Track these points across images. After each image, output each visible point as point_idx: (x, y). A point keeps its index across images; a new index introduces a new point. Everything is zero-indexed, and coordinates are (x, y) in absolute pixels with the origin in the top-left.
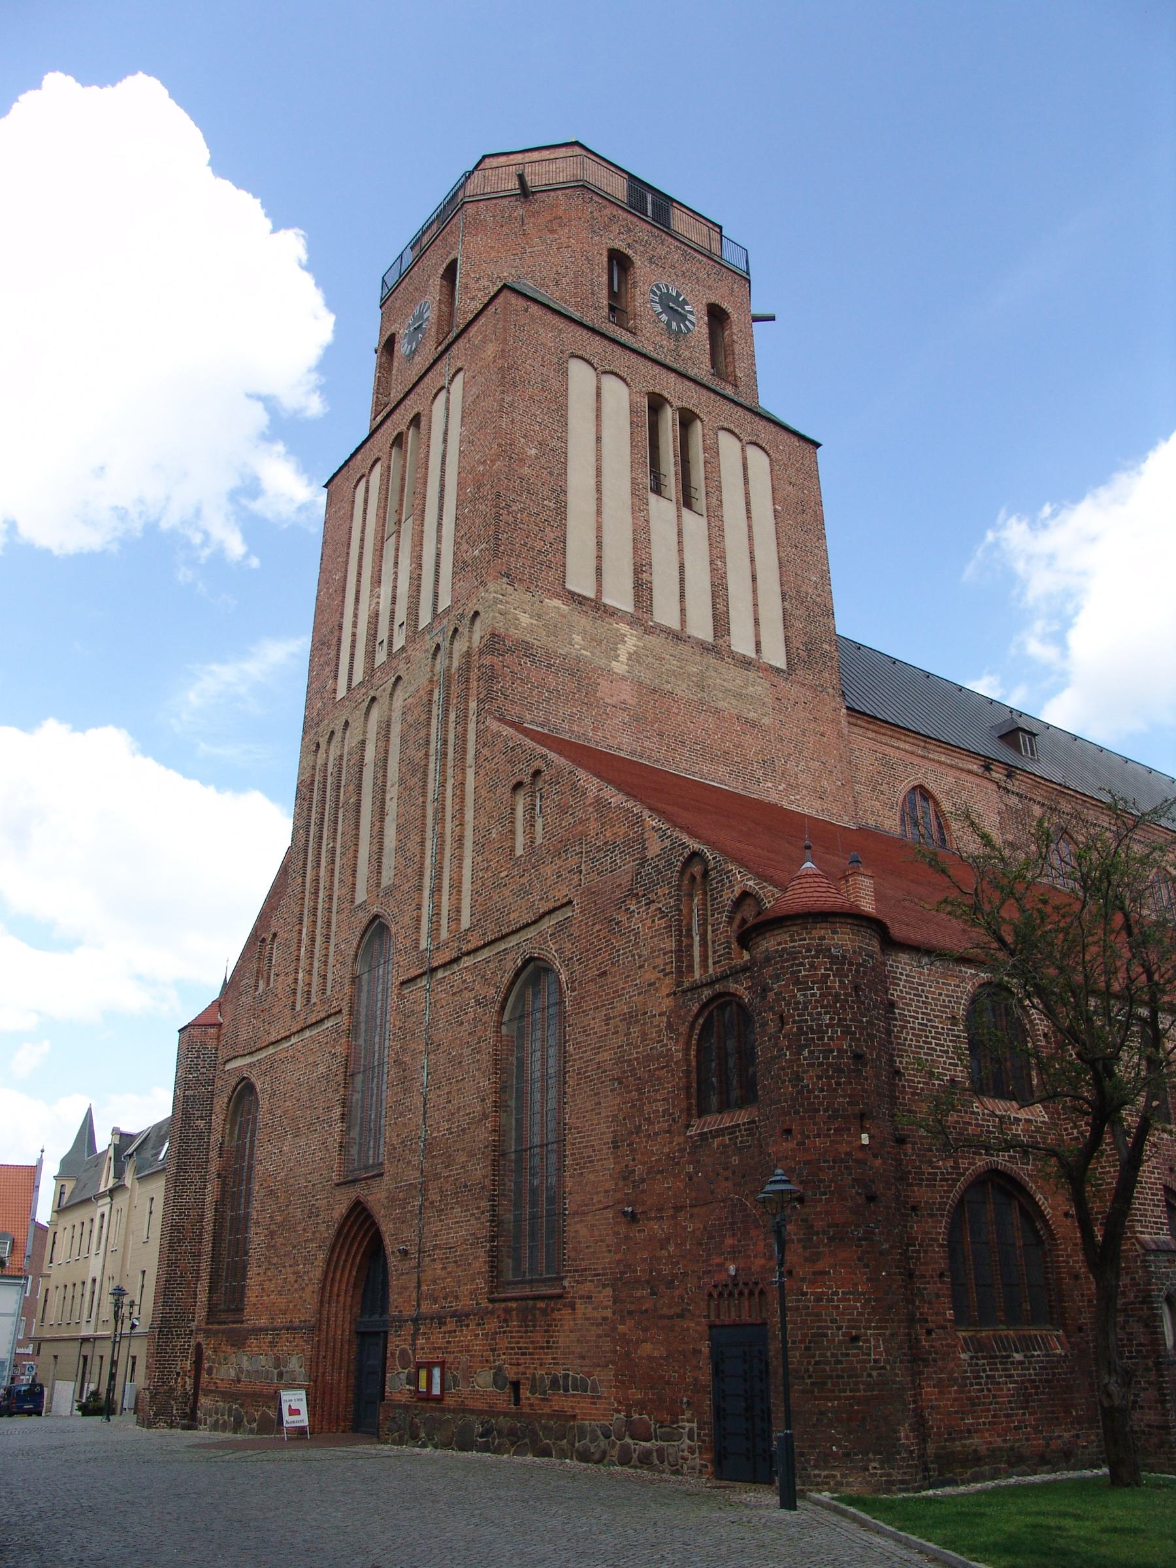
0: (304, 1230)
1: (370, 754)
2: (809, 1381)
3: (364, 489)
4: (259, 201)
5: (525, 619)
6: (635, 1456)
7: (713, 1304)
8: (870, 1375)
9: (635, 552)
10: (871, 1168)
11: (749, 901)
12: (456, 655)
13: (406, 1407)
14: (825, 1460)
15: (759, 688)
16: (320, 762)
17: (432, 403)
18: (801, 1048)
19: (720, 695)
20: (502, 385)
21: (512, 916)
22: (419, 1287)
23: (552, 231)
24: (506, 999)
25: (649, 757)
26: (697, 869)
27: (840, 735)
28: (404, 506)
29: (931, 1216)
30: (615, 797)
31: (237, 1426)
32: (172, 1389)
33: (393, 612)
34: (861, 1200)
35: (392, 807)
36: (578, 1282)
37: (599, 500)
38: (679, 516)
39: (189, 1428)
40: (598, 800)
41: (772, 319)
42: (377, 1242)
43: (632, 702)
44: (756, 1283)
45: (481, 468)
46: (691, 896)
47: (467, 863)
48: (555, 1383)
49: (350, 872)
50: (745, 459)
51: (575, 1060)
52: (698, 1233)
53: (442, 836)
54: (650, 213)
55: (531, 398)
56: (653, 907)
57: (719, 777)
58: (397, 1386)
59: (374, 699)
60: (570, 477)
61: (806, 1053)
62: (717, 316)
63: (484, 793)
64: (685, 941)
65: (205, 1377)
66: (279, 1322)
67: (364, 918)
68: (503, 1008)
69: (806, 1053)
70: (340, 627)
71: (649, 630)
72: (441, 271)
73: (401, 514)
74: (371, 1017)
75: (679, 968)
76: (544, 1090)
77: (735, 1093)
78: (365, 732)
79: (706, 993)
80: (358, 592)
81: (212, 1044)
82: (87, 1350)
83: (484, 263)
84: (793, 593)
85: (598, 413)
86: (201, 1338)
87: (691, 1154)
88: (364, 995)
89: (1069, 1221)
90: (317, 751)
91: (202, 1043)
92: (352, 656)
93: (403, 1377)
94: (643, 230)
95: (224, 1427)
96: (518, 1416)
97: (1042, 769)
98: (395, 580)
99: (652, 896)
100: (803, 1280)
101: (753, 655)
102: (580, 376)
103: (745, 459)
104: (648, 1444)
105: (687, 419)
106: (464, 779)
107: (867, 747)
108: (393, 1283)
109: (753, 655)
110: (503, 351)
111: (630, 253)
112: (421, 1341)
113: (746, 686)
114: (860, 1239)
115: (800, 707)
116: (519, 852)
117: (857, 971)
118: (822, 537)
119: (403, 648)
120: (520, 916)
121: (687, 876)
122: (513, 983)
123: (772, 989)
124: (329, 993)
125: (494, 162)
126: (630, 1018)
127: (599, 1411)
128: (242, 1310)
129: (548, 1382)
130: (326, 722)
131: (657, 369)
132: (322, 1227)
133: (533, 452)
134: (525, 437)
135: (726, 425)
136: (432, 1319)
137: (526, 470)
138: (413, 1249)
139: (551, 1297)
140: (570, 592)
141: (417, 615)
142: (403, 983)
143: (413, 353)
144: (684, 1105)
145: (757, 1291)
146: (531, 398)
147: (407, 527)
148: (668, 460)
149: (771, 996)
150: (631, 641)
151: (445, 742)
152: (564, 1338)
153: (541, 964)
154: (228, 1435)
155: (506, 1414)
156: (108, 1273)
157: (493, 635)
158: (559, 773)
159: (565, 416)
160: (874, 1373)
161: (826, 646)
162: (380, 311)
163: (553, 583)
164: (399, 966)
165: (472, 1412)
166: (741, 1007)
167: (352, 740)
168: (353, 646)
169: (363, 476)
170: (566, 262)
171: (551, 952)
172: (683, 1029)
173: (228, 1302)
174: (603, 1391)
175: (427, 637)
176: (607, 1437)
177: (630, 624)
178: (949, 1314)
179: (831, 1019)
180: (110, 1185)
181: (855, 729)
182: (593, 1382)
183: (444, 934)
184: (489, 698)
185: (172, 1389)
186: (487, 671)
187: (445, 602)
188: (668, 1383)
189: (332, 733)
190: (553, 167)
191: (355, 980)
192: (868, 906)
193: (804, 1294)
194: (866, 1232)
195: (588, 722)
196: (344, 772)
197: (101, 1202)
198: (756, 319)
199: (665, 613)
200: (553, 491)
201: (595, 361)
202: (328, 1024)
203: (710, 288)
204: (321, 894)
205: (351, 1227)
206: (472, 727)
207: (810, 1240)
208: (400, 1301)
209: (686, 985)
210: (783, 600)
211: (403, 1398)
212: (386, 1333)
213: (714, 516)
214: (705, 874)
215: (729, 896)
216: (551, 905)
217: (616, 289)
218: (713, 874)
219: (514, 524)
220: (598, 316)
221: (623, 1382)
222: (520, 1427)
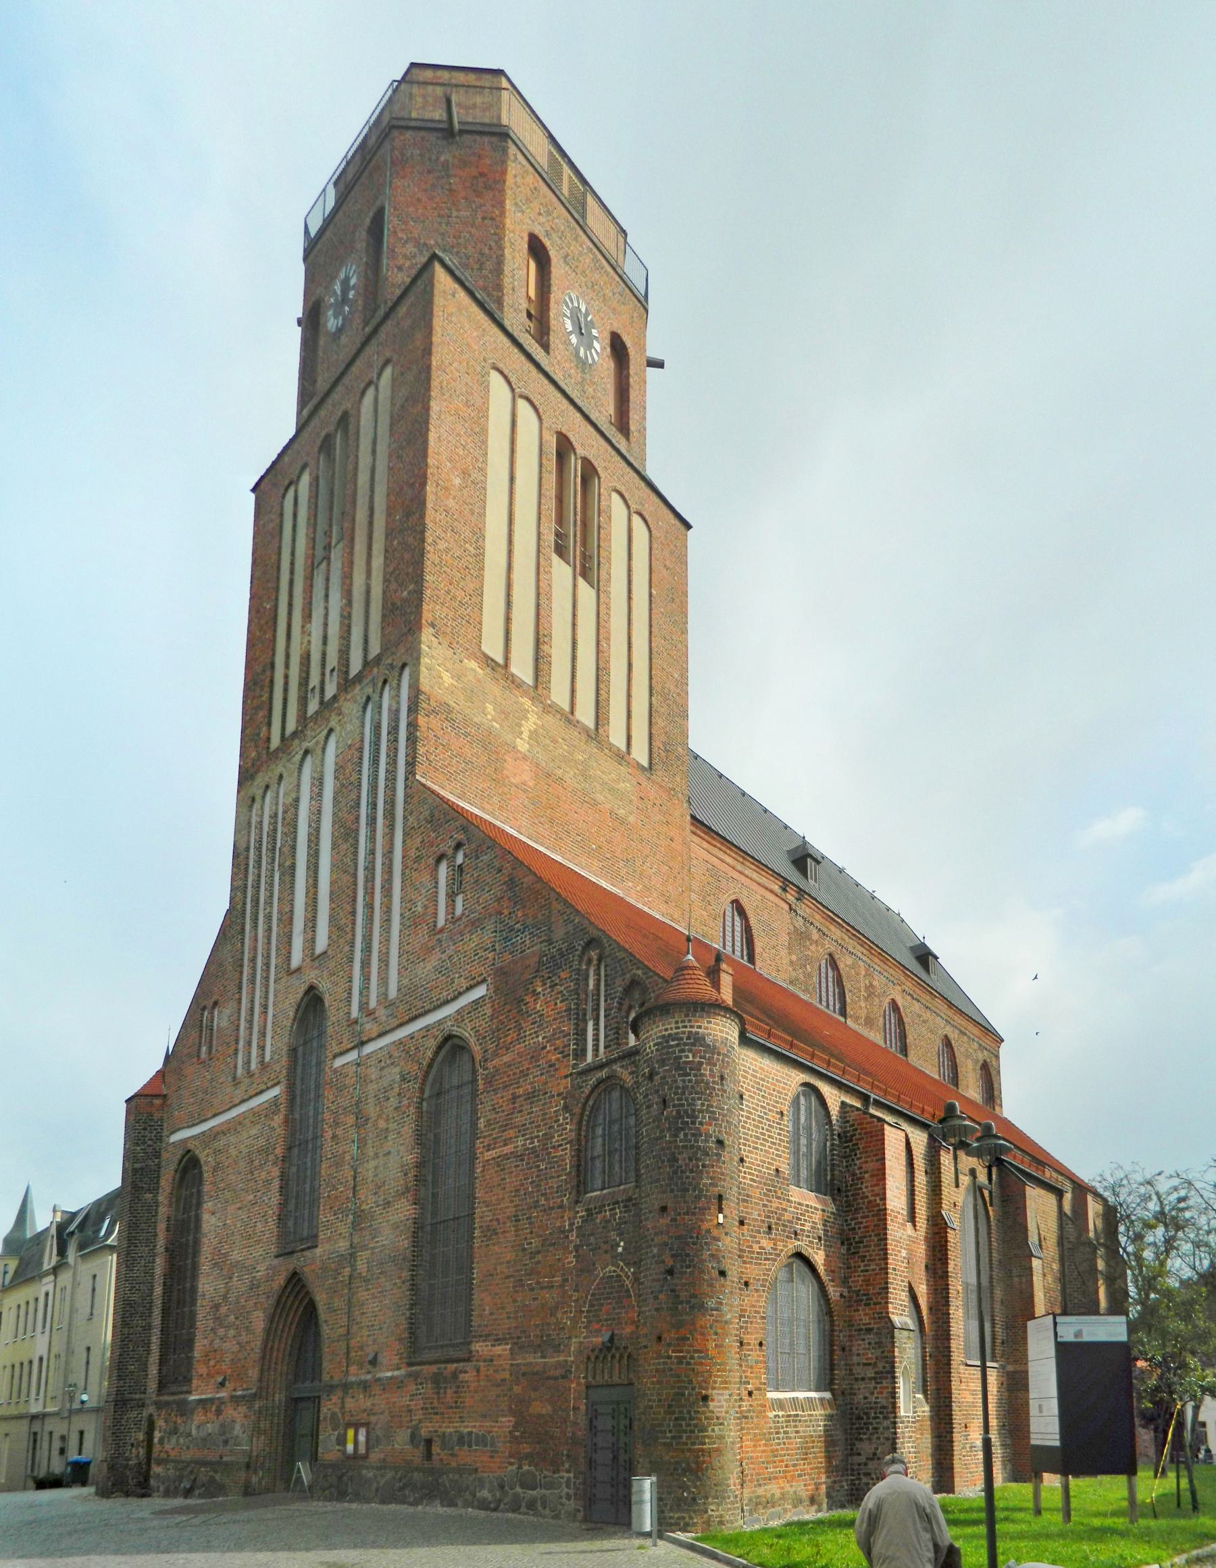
2: (669, 1435)
5: (447, 679)
7: (591, 1366)
29: (757, 1291)
33: (324, 654)
42: (311, 1311)
43: (531, 784)
51: (485, 1137)
70: (273, 666)
73: (331, 537)
82: (36, 1427)
86: (152, 1409)
90: (251, 807)
91: (147, 1113)
92: (285, 700)
93: (334, 1438)
100: (669, 1345)
104: (534, 1493)
115: (656, 809)
116: (441, 922)
118: (684, 632)
121: (585, 958)
123: (657, 1073)
129: (455, 1438)
132: (263, 1299)
133: (457, 481)
135: (618, 487)
141: (348, 660)
143: (340, 330)
144: (574, 1182)
147: (336, 555)
149: (657, 1078)
153: (456, 1041)
156: (54, 1351)
159: (485, 442)
163: (470, 641)
168: (286, 690)
172: (577, 1110)
180: (53, 1263)
181: (696, 839)
182: (492, 1437)
193: (669, 1357)
197: (45, 1280)
199: (559, 695)
208: (331, 1369)
212: (319, 1397)
221: (516, 1438)
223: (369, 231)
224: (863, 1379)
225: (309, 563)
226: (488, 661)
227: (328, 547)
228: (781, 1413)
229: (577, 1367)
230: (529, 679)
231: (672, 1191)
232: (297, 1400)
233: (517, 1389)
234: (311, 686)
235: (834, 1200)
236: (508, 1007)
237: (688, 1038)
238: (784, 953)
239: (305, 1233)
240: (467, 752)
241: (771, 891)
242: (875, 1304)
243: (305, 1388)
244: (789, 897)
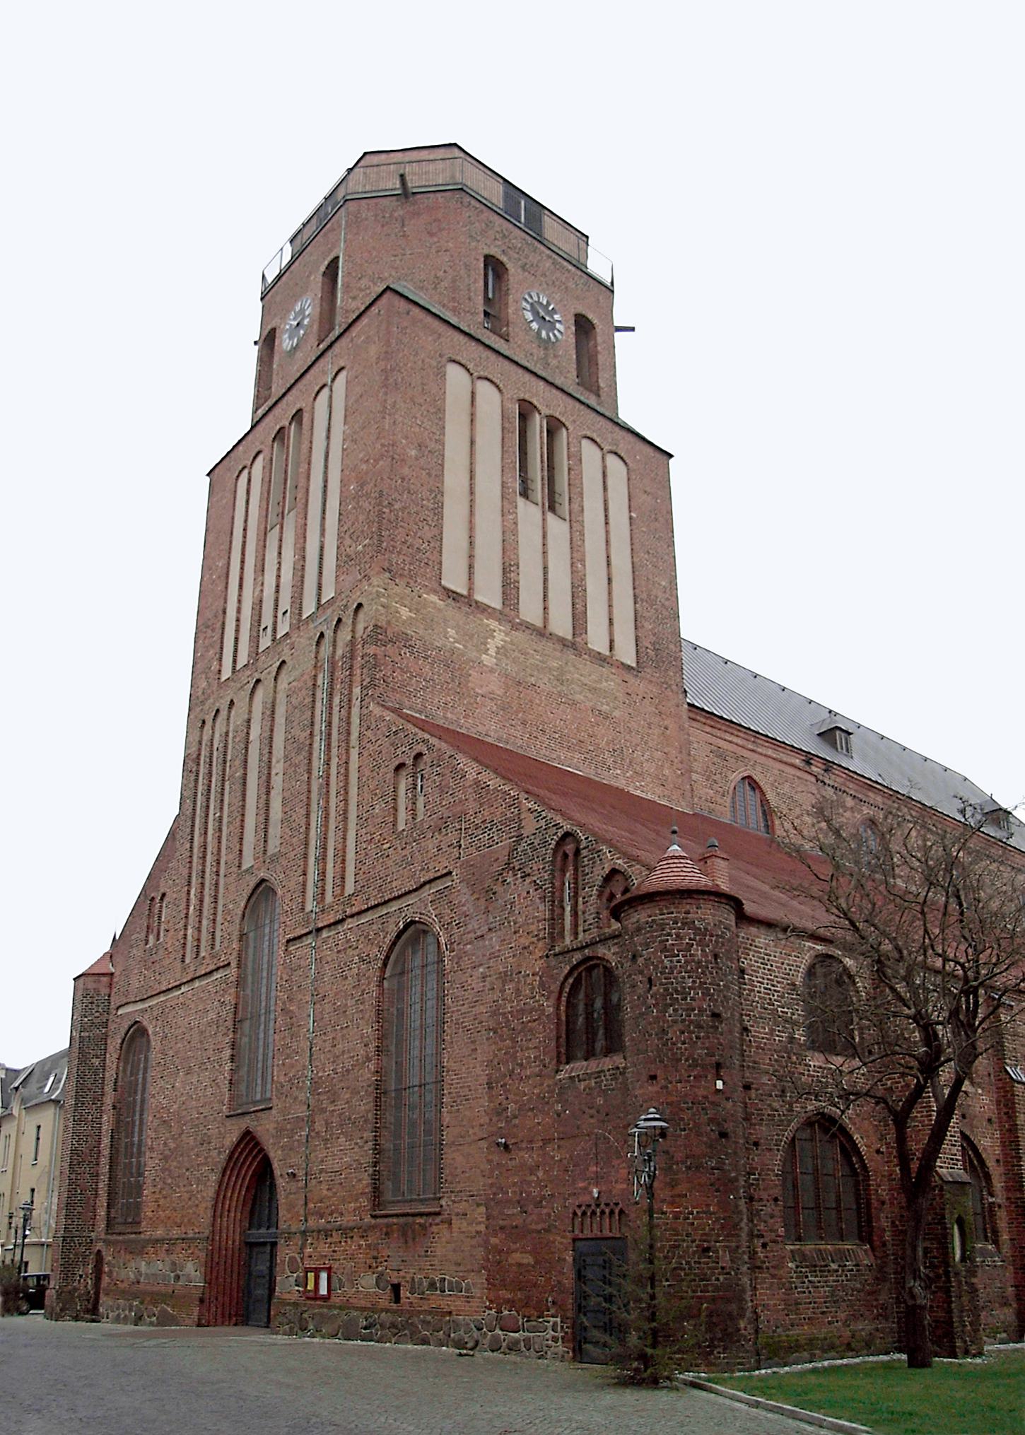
0: (197, 1155)
3: (246, 480)
5: (405, 613)
6: (504, 1344)
8: (718, 1279)
10: (724, 1109)
11: (618, 877)
12: (340, 644)
13: (295, 1305)
15: (611, 682)
16: (206, 738)
17: (315, 399)
19: (578, 689)
20: (386, 386)
21: (394, 884)
23: (431, 234)
24: (387, 957)
26: (569, 848)
27: (681, 728)
28: (286, 498)
30: (494, 782)
31: (138, 1320)
33: (277, 600)
34: (715, 1136)
35: (277, 782)
36: (454, 1202)
39: (93, 1321)
40: (477, 782)
41: (632, 329)
42: (266, 1165)
43: (500, 692)
44: (617, 1204)
45: (364, 467)
46: (563, 871)
48: (432, 1285)
49: (237, 839)
52: (565, 1162)
53: (326, 809)
54: (523, 219)
56: (528, 880)
57: (574, 763)
58: (287, 1286)
59: (258, 681)
62: (583, 326)
63: (367, 773)
64: (557, 911)
65: (105, 1280)
66: (175, 1233)
68: (385, 964)
71: (515, 627)
72: (323, 269)
73: (284, 507)
74: (257, 970)
75: (551, 934)
76: (423, 1038)
77: (600, 1043)
78: (250, 712)
79: (577, 957)
81: (104, 991)
83: (366, 264)
84: (644, 596)
85: (472, 418)
87: (559, 1094)
88: (251, 951)
89: (879, 1157)
91: (94, 992)
93: (292, 1280)
95: (126, 1320)
97: (855, 765)
99: (528, 870)
101: (608, 653)
105: (554, 426)
106: (348, 758)
109: (608, 653)
110: (386, 352)
111: (504, 259)
112: (308, 1250)
113: (600, 681)
114: (713, 1168)
115: (647, 701)
120: (399, 886)
122: (394, 944)
124: (217, 947)
125: (375, 159)
126: (505, 977)
127: (471, 1306)
128: (139, 1223)
130: (211, 700)
131: (527, 376)
132: (214, 1153)
133: (413, 453)
134: (407, 438)
135: (589, 434)
136: (319, 1231)
137: (406, 471)
138: (301, 1173)
140: (445, 588)
142: (288, 941)
143: (295, 349)
145: (617, 1211)
148: (536, 465)
149: (640, 961)
150: (500, 636)
151: (329, 724)
152: (440, 1250)
153: (421, 927)
154: (130, 1327)
155: (387, 1311)
157: (376, 626)
159: (442, 419)
161: (672, 646)
162: (260, 305)
164: (284, 923)
165: (357, 1309)
166: (608, 971)
167: (238, 716)
169: (244, 468)
170: (442, 266)
171: (431, 915)
172: (555, 987)
173: (125, 1215)
174: (476, 1292)
175: (312, 626)
176: (479, 1329)
177: (499, 620)
178: (781, 1231)
179: (694, 982)
181: (695, 724)
183: (329, 898)
184: (372, 685)
186: (363, 658)
187: (328, 594)
189: (218, 711)
190: (431, 167)
191: (242, 937)
192: (725, 887)
193: (664, 1213)
195: (460, 709)
196: (230, 747)
198: (619, 329)
199: (530, 610)
201: (470, 366)
202: (217, 975)
203: (577, 298)
204: (209, 857)
205: (241, 1153)
206: (355, 711)
207: (671, 1168)
208: (287, 1218)
209: (557, 949)
211: (294, 1298)
212: (274, 1244)
214: (577, 852)
215: (598, 874)
216: (431, 875)
217: (490, 296)
218: (584, 853)
219: (392, 523)
220: (474, 322)
222: (398, 1318)
225: (262, 527)
226: (451, 595)
227: (282, 515)
230: (496, 603)
232: (251, 1245)
233: (494, 1240)
234: (263, 626)
239: (258, 1097)
241: (792, 765)
243: (261, 1233)
244: (814, 768)
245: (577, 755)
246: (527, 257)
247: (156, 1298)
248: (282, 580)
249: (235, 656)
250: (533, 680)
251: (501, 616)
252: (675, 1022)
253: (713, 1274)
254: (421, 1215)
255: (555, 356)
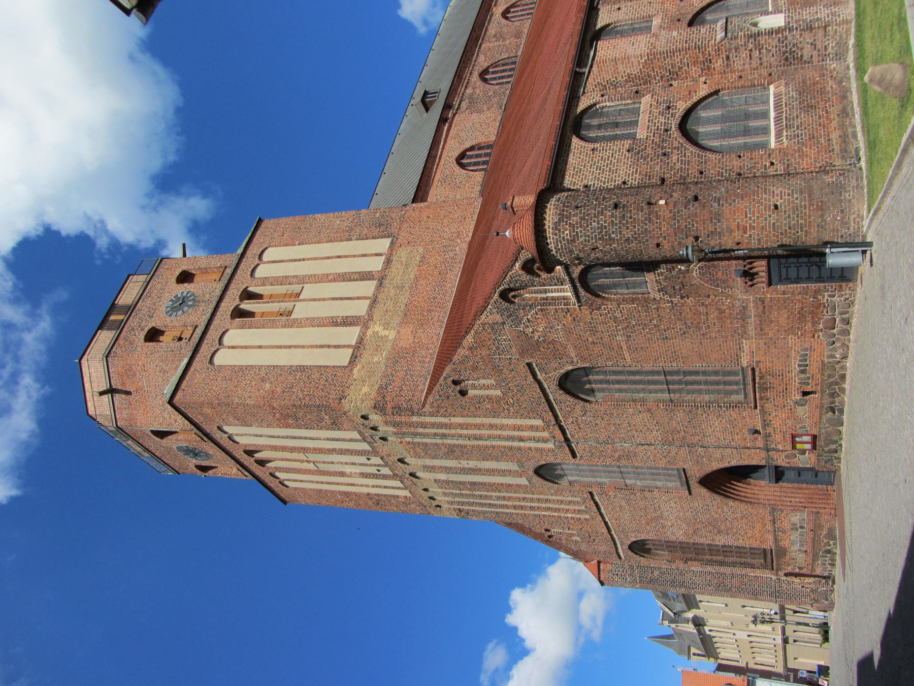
1: (443, 477)
4: (511, 620)
5: (365, 389)
6: (844, 327)
9: (326, 326)
14: (844, 223)
15: (402, 254)
18: (610, 239)
22: (748, 448)
23: (134, 375)
25: (444, 317)
29: (706, 163)
32: (812, 591)
34: (697, 204)
35: (472, 464)
37: (295, 347)
38: (304, 300)
45: (277, 415)
47: (505, 421)
50: (269, 262)
55: (235, 387)
58: (807, 460)
60: (282, 364)
61: (613, 236)
65: (804, 571)
66: (769, 527)
67: (536, 480)
69: (613, 236)
72: (158, 439)
80: (348, 484)
86: (781, 573)
92: (386, 487)
93: (801, 457)
94: (133, 322)
96: (823, 392)
98: (342, 463)
101: (384, 257)
102: (223, 358)
103: (269, 262)
107: (436, 193)
108: (746, 463)
109: (384, 257)
111: (147, 329)
112: (780, 447)
117: (567, 207)
119: (382, 458)
124: (579, 499)
128: (765, 550)
129: (802, 376)
132: (715, 503)
133: (268, 385)
134: (259, 390)
137: (279, 390)
139: (754, 374)
140: (350, 363)
146: (235, 387)
149: (581, 255)
150: (376, 328)
151: (436, 434)
158: (454, 370)
160: (795, 196)
161: (377, 215)
177: (367, 328)
182: (802, 350)
185: (812, 591)
188: (802, 309)
192: (530, 200)
193: (750, 236)
194: (715, 202)
195: (423, 353)
199: (360, 309)
200: (291, 373)
201: (213, 350)
203: (167, 282)
207: (719, 233)
210: (351, 240)
213: (303, 280)
218: (512, 285)
221: (802, 335)
222: (827, 391)
223: (162, 438)
224: (760, 59)
226: (354, 359)
228: (785, 134)
229: (757, 293)
231: (647, 241)
235: (643, 96)
236: (542, 349)
237: (556, 234)
238: (483, 116)
240: (401, 374)
242: (710, 55)
245: (448, 276)
246: (144, 315)
247: (815, 541)
248: (348, 461)
249: (396, 488)
250: (403, 306)
251: (366, 327)
252: (620, 232)
253: (793, 202)
254: (754, 380)
255: (204, 296)
